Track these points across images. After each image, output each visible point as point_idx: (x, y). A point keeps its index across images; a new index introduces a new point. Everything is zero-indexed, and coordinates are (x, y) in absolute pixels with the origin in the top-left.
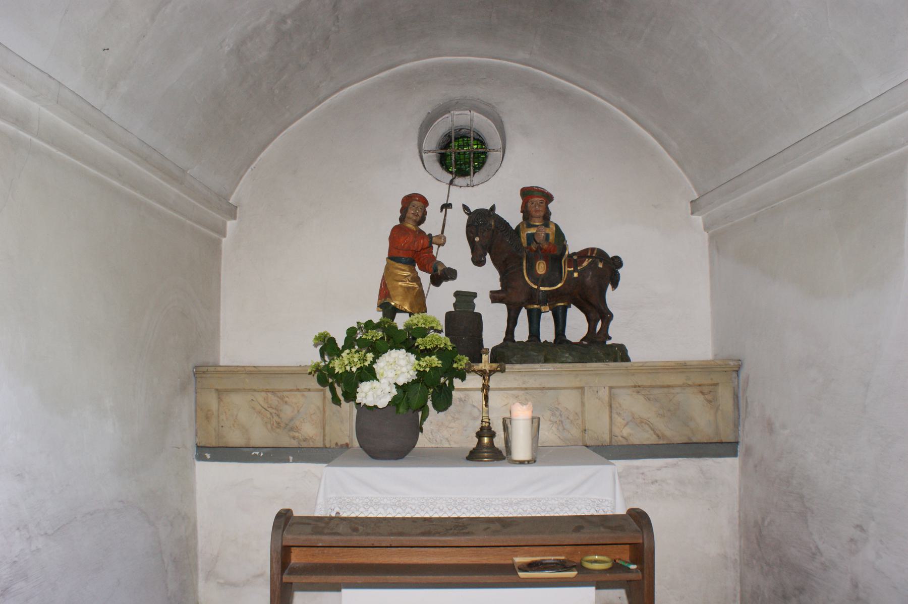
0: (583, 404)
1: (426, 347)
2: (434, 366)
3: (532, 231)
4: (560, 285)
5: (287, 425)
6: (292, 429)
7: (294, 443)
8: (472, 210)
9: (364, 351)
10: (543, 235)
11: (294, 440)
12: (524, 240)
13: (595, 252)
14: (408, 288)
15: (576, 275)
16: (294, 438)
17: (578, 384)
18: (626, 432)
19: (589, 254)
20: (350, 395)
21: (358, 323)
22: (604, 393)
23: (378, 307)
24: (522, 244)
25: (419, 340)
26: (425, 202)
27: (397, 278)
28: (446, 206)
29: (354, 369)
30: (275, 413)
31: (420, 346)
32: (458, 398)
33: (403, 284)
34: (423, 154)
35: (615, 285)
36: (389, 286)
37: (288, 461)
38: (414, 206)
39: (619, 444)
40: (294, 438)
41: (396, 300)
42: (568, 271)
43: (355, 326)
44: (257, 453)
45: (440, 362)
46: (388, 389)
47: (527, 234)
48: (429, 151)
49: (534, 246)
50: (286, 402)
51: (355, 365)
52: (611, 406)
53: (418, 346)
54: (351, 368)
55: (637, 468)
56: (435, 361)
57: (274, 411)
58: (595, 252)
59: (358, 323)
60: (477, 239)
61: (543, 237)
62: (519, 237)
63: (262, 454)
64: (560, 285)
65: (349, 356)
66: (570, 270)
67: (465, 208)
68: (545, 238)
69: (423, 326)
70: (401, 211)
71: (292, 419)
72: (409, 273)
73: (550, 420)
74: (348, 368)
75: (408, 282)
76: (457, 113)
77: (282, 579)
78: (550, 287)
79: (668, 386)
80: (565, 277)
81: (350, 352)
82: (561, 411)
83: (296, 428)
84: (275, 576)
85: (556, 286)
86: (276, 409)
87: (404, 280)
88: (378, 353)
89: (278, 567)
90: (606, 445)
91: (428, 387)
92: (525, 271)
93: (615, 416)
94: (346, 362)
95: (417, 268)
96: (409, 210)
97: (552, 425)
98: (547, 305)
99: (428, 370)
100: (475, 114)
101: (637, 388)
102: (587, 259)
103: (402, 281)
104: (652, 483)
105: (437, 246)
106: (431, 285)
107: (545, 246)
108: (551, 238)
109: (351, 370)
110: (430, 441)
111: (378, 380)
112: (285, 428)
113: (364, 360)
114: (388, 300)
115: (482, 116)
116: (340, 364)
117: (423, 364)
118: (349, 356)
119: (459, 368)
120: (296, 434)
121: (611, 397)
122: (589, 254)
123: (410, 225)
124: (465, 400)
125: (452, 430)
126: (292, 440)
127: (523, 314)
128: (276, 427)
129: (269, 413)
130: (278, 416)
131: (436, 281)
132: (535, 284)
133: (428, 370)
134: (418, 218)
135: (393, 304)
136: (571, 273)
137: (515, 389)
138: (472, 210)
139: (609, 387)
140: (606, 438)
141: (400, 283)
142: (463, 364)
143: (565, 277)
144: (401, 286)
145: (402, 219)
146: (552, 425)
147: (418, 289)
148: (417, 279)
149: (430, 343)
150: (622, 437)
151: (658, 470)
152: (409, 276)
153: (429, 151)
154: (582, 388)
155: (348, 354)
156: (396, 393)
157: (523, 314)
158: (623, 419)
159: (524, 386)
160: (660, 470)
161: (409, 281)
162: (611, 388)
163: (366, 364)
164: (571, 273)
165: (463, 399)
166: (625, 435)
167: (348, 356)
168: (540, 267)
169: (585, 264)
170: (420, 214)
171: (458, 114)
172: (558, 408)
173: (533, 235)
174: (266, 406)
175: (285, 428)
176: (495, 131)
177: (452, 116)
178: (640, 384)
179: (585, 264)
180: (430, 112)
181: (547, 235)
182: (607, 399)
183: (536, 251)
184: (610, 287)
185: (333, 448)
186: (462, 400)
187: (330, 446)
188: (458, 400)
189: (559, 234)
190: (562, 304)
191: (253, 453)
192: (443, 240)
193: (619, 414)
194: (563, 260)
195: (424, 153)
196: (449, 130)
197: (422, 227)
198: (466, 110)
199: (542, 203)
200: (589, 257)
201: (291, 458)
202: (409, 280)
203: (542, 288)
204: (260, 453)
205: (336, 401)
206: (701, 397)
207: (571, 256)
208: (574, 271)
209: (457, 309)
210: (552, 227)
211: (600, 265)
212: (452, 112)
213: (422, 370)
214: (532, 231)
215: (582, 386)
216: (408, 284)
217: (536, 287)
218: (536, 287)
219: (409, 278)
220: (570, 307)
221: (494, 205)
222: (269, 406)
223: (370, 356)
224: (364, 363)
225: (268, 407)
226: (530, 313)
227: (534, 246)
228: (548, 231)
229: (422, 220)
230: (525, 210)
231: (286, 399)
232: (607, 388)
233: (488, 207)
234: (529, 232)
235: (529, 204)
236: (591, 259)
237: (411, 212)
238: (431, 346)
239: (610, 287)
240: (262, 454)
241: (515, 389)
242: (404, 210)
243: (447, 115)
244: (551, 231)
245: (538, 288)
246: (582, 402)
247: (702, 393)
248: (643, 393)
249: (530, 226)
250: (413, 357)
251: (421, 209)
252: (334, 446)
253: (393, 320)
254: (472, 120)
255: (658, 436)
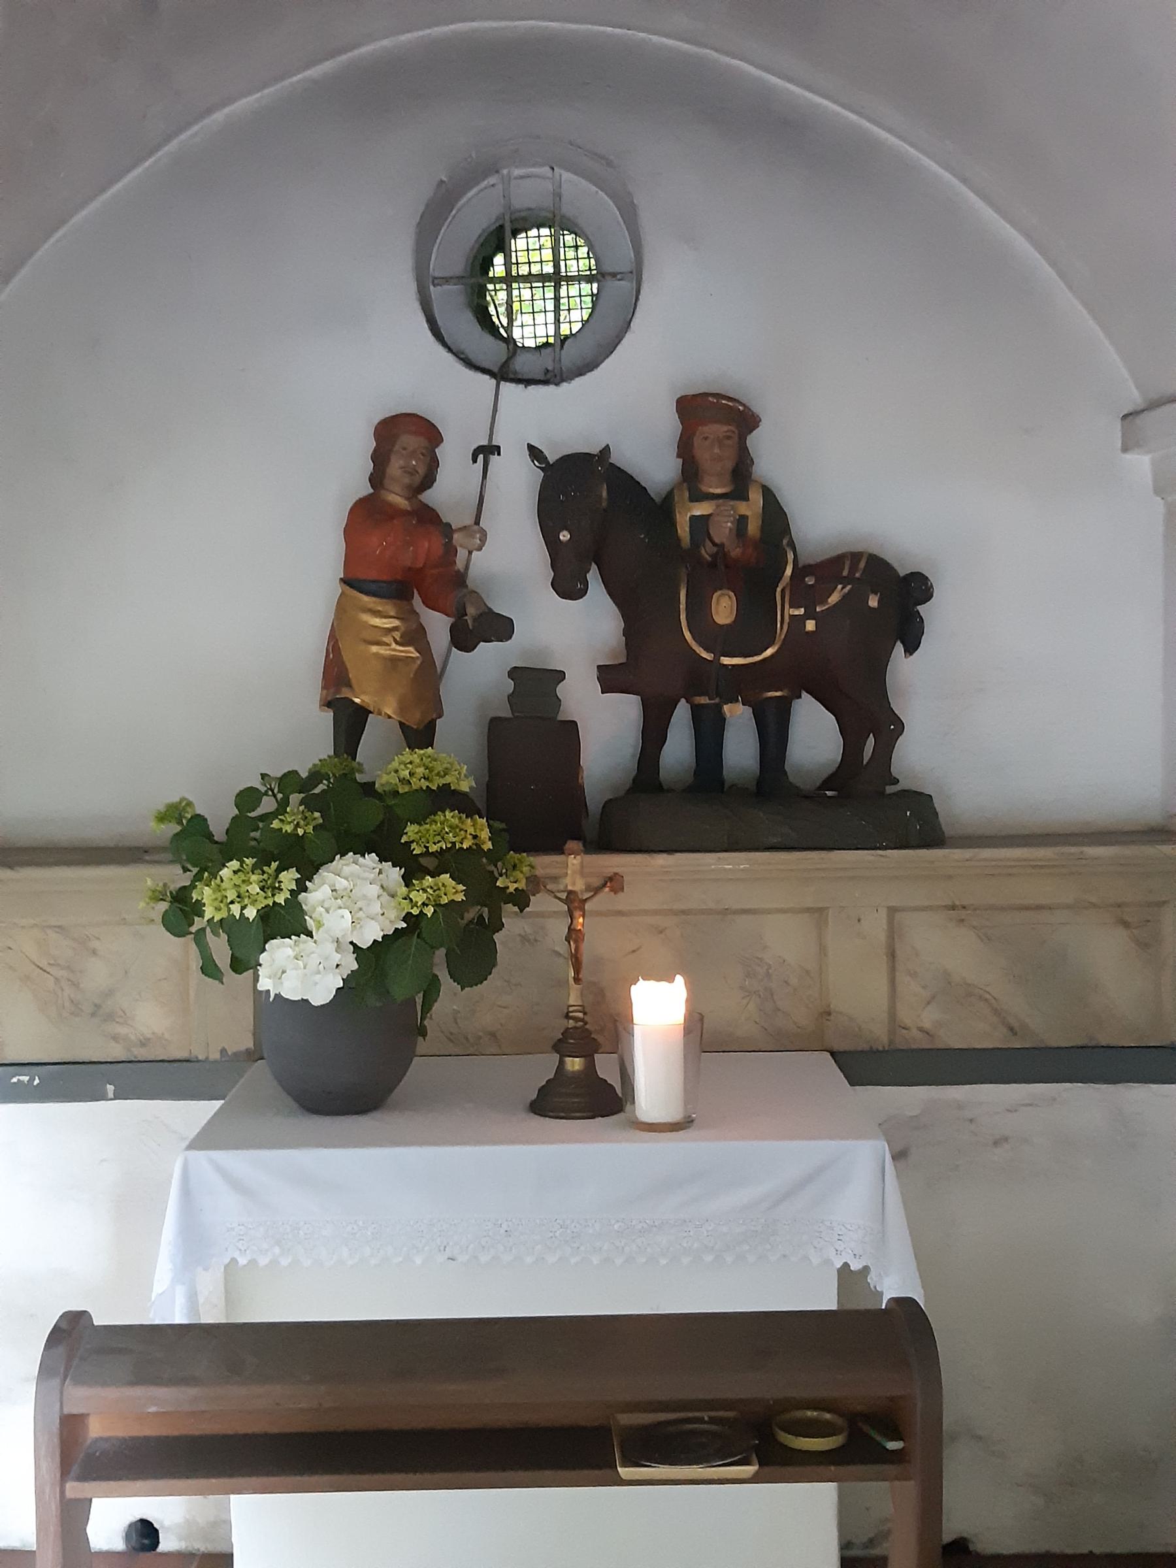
0: (822, 950)
1: (427, 848)
2: (445, 900)
3: (701, 509)
4: (769, 652)
5: (98, 1006)
6: (110, 1017)
7: (116, 1052)
8: (552, 458)
9: (274, 865)
10: (729, 524)
11: (117, 1042)
12: (683, 530)
13: (862, 565)
14: (394, 661)
15: (810, 625)
16: (115, 1038)
17: (809, 902)
18: (929, 1018)
19: (845, 573)
20: (244, 963)
21: (263, 776)
22: (876, 925)
23: (321, 706)
24: (679, 540)
25: (412, 830)
26: (430, 434)
27: (368, 635)
28: (488, 451)
29: (251, 913)
30: (69, 980)
31: (414, 846)
32: (520, 935)
33: (382, 652)
34: (432, 287)
35: (911, 647)
36: (347, 656)
37: (100, 1096)
38: (404, 449)
39: (914, 1047)
40: (115, 1038)
41: (364, 693)
42: (791, 616)
43: (257, 783)
44: (26, 1079)
45: (461, 887)
46: (337, 958)
47: (693, 518)
48: (447, 280)
49: (707, 551)
50: (94, 952)
51: (254, 902)
52: (892, 955)
53: (408, 844)
54: (243, 908)
55: (960, 1106)
56: (451, 889)
57: (64, 973)
58: (862, 565)
59: (263, 776)
60: (564, 536)
61: (730, 529)
62: (673, 524)
63: (37, 1081)
64: (769, 652)
65: (237, 880)
66: (796, 612)
67: (534, 452)
68: (734, 532)
69: (424, 784)
70: (375, 457)
71: (110, 993)
72: (396, 623)
73: (742, 988)
74: (236, 909)
75: (394, 646)
76: (517, 172)
77: (62, 1492)
78: (745, 656)
79: (1039, 908)
80: (782, 631)
81: (242, 866)
82: (770, 967)
83: (121, 1013)
84: (47, 1490)
85: (760, 654)
86: (68, 967)
87: (385, 639)
88: (308, 871)
89: (52, 1467)
90: (881, 1048)
91: (434, 948)
92: (683, 617)
93: (901, 977)
94: (231, 895)
95: (417, 601)
96: (393, 458)
97: (745, 1001)
98: (737, 701)
99: (429, 911)
100: (566, 175)
101: (956, 910)
102: (840, 587)
103: (378, 643)
104: (996, 1143)
105: (532, 273)
106: (454, 649)
107: (735, 552)
108: (753, 528)
109: (242, 914)
110: (451, 1041)
111: (310, 934)
112: (93, 1015)
113: (274, 888)
114: (345, 693)
115: (583, 182)
116: (216, 899)
117: (419, 897)
118: (237, 880)
119: (511, 889)
120: (122, 1030)
121: (893, 932)
122: (845, 573)
123: (397, 499)
124: (536, 941)
125: (506, 1011)
126: (113, 1044)
127: (682, 713)
128: (72, 1014)
129: (52, 978)
130: (75, 985)
131: (463, 639)
132: (707, 650)
133: (429, 911)
134: (417, 479)
135: (357, 700)
136: (801, 620)
137: (656, 912)
138: (552, 458)
139: (888, 907)
140: (885, 1040)
141: (374, 649)
142: (520, 876)
143: (782, 631)
144: (376, 655)
145: (377, 479)
146: (745, 1001)
147: (419, 662)
148: (416, 636)
149: (439, 838)
150: (921, 1029)
151: (1008, 1111)
152: (395, 629)
153: (447, 280)
154: (821, 910)
155: (235, 872)
156: (355, 966)
157: (682, 713)
158: (924, 987)
159: (678, 906)
160: (1016, 1111)
161: (397, 643)
162: (892, 911)
163: (280, 899)
164: (797, 622)
165: (531, 937)
166: (927, 1025)
167: (235, 878)
168: (721, 608)
169: (834, 599)
170: (422, 471)
171: (522, 177)
172: (761, 959)
173: (705, 518)
174: (43, 963)
175: (93, 1015)
176: (618, 222)
177: (506, 181)
178: (965, 903)
179: (834, 599)
180: (444, 179)
181: (742, 520)
182: (882, 937)
183: (713, 565)
184: (899, 648)
185: (215, 1062)
186: (529, 941)
187: (207, 1058)
188: (518, 939)
189: (775, 513)
190: (778, 694)
191: (15, 1080)
192: (478, 542)
193: (913, 975)
194: (779, 589)
195: (434, 286)
196: (498, 219)
197: (428, 497)
198: (542, 165)
199: (728, 438)
200: (845, 581)
201: (110, 1088)
202: (395, 640)
203: (726, 661)
204: (32, 1080)
205: (209, 969)
206: (1121, 933)
207: (801, 572)
208: (808, 615)
209: (516, 714)
210: (756, 497)
211: (873, 602)
212: (505, 172)
213: (415, 911)
214: (701, 509)
215: (820, 905)
216: (395, 650)
217: (708, 656)
218: (708, 656)
219: (397, 635)
220: (800, 697)
221: (608, 445)
222: (52, 962)
223: (289, 878)
224: (273, 895)
225: (49, 964)
226: (696, 711)
227: (707, 551)
228: (743, 508)
229: (428, 480)
230: (685, 449)
231: (95, 944)
232: (883, 913)
233: (595, 450)
234: (698, 513)
235: (697, 441)
236: (849, 587)
237: (395, 467)
238: (439, 845)
239: (899, 648)
240: (37, 1081)
241: (656, 912)
242: (380, 458)
243: (492, 180)
244: (752, 507)
245: (716, 658)
246: (820, 944)
247: (1126, 925)
248: (975, 923)
249: (698, 496)
250: (394, 874)
251: (423, 455)
252: (217, 1056)
253: (354, 759)
254: (558, 195)
255: (1011, 1029)
